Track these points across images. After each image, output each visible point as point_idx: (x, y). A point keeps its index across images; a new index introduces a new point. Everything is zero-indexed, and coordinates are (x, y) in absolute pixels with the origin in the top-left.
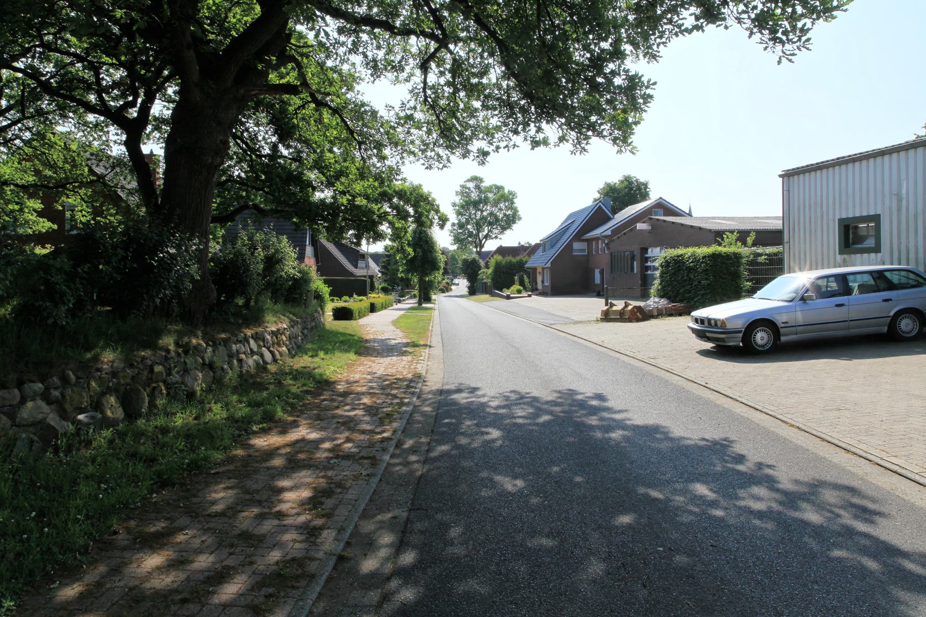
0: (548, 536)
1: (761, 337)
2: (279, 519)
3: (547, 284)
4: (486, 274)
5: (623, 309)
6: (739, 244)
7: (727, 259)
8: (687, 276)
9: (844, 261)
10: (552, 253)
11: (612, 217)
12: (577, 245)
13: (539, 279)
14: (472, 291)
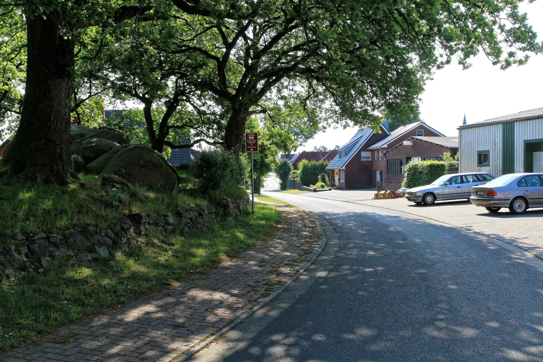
1: (429, 199)
3: (342, 181)
4: (296, 174)
6: (451, 158)
7: (438, 168)
8: (419, 176)
9: (479, 169)
10: (346, 159)
11: (389, 134)
12: (364, 154)
13: (336, 178)
14: (284, 187)
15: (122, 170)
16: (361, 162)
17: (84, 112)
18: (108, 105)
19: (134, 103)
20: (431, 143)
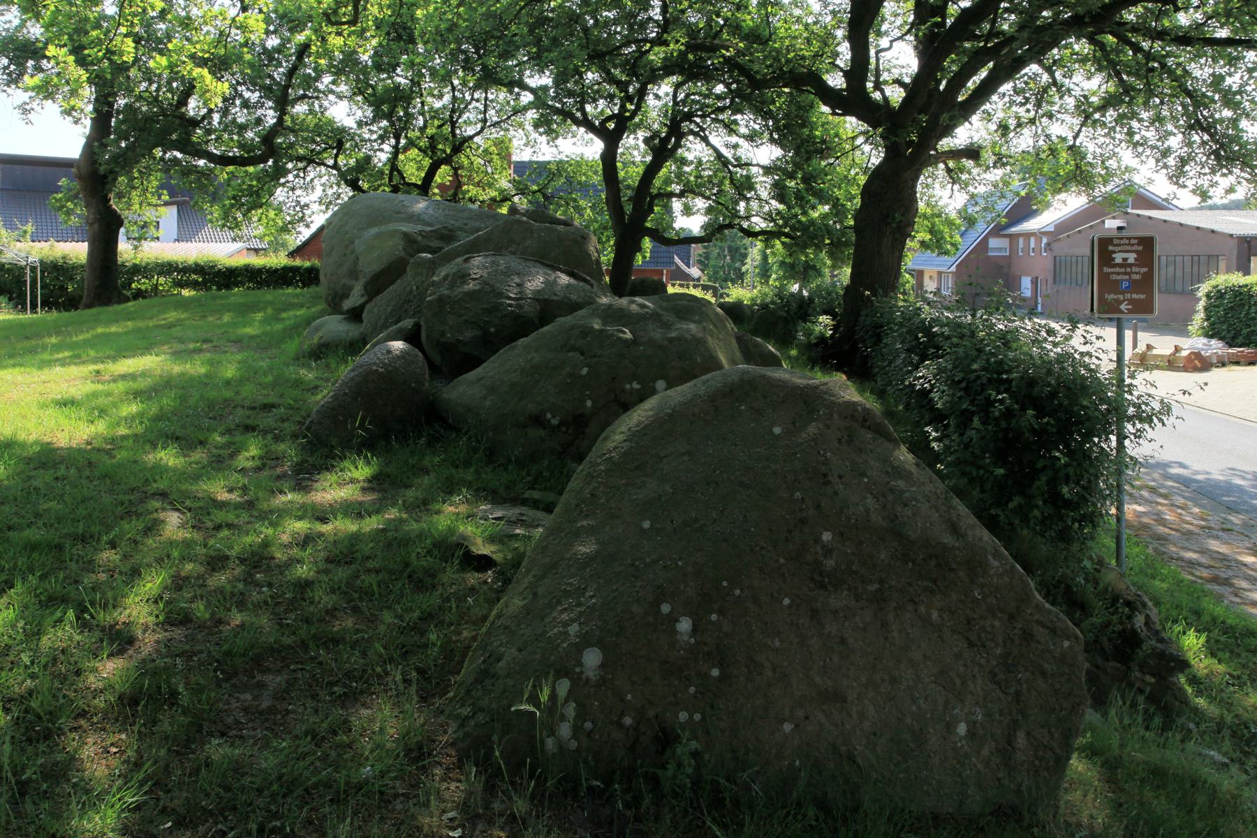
0: (300, 518)
2: (138, 515)
5: (1173, 354)
12: (994, 243)
15: (673, 619)
16: (989, 258)
17: (472, 163)
18: (523, 148)
19: (574, 144)
20: (1181, 225)
